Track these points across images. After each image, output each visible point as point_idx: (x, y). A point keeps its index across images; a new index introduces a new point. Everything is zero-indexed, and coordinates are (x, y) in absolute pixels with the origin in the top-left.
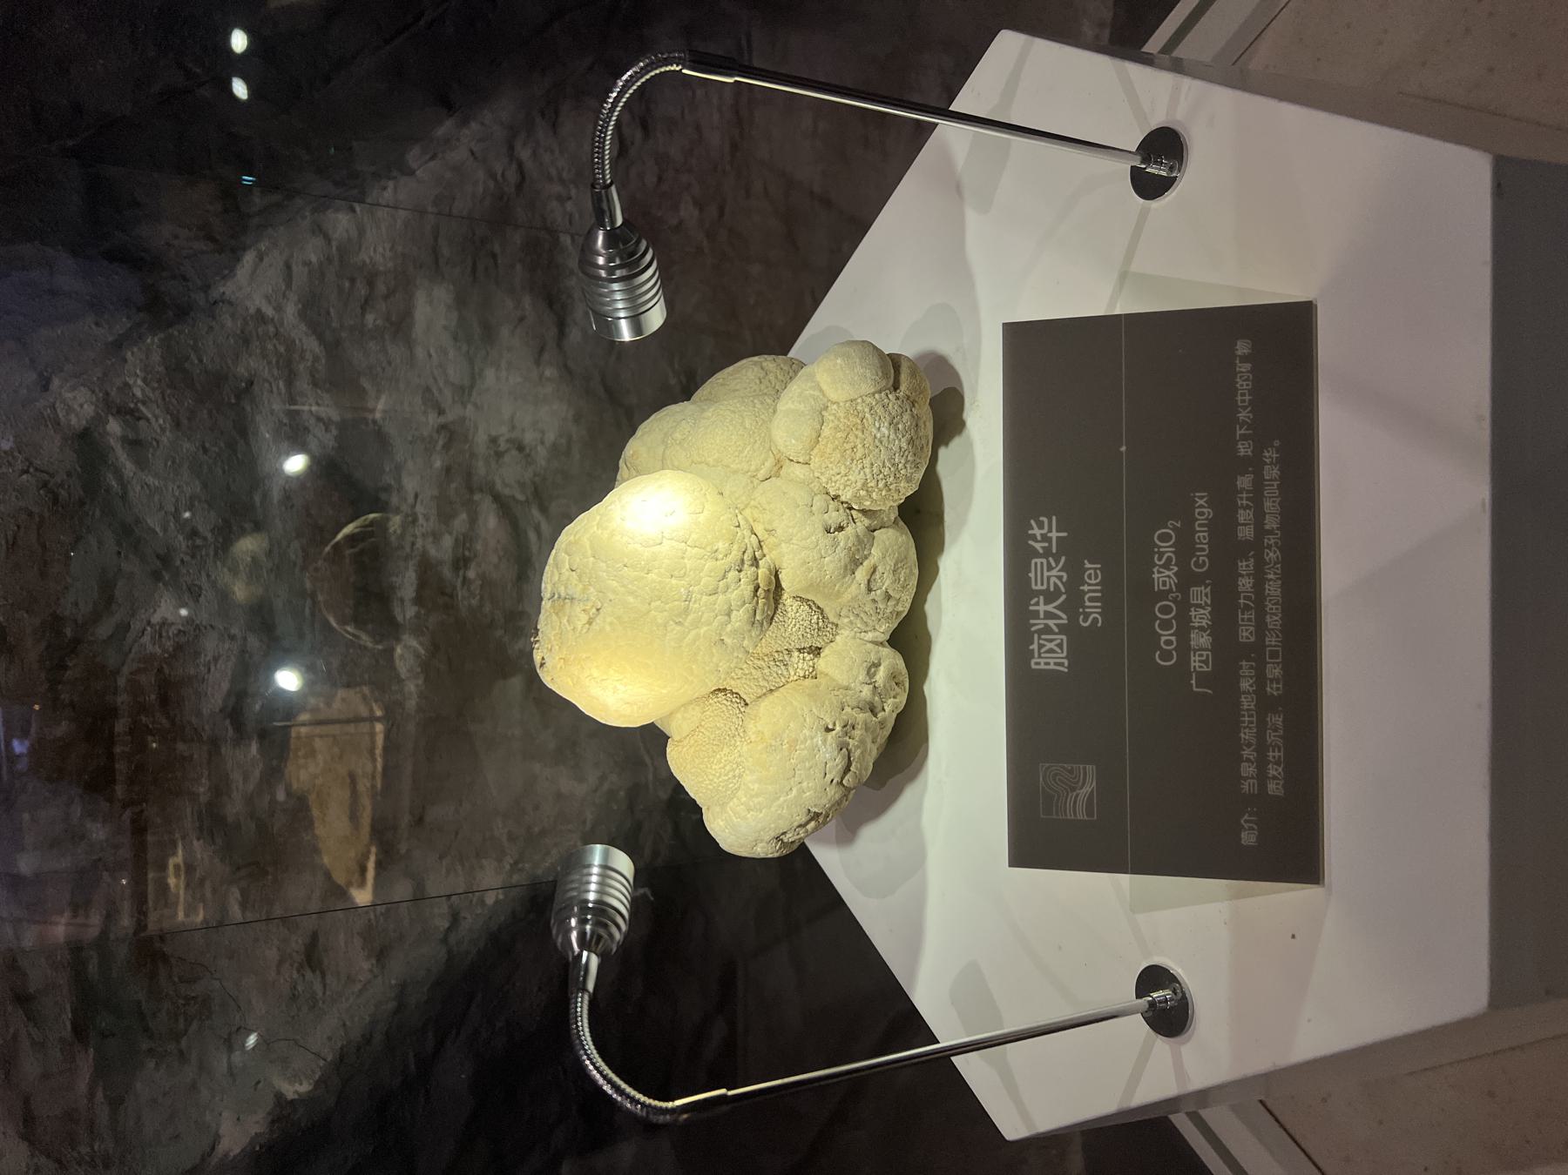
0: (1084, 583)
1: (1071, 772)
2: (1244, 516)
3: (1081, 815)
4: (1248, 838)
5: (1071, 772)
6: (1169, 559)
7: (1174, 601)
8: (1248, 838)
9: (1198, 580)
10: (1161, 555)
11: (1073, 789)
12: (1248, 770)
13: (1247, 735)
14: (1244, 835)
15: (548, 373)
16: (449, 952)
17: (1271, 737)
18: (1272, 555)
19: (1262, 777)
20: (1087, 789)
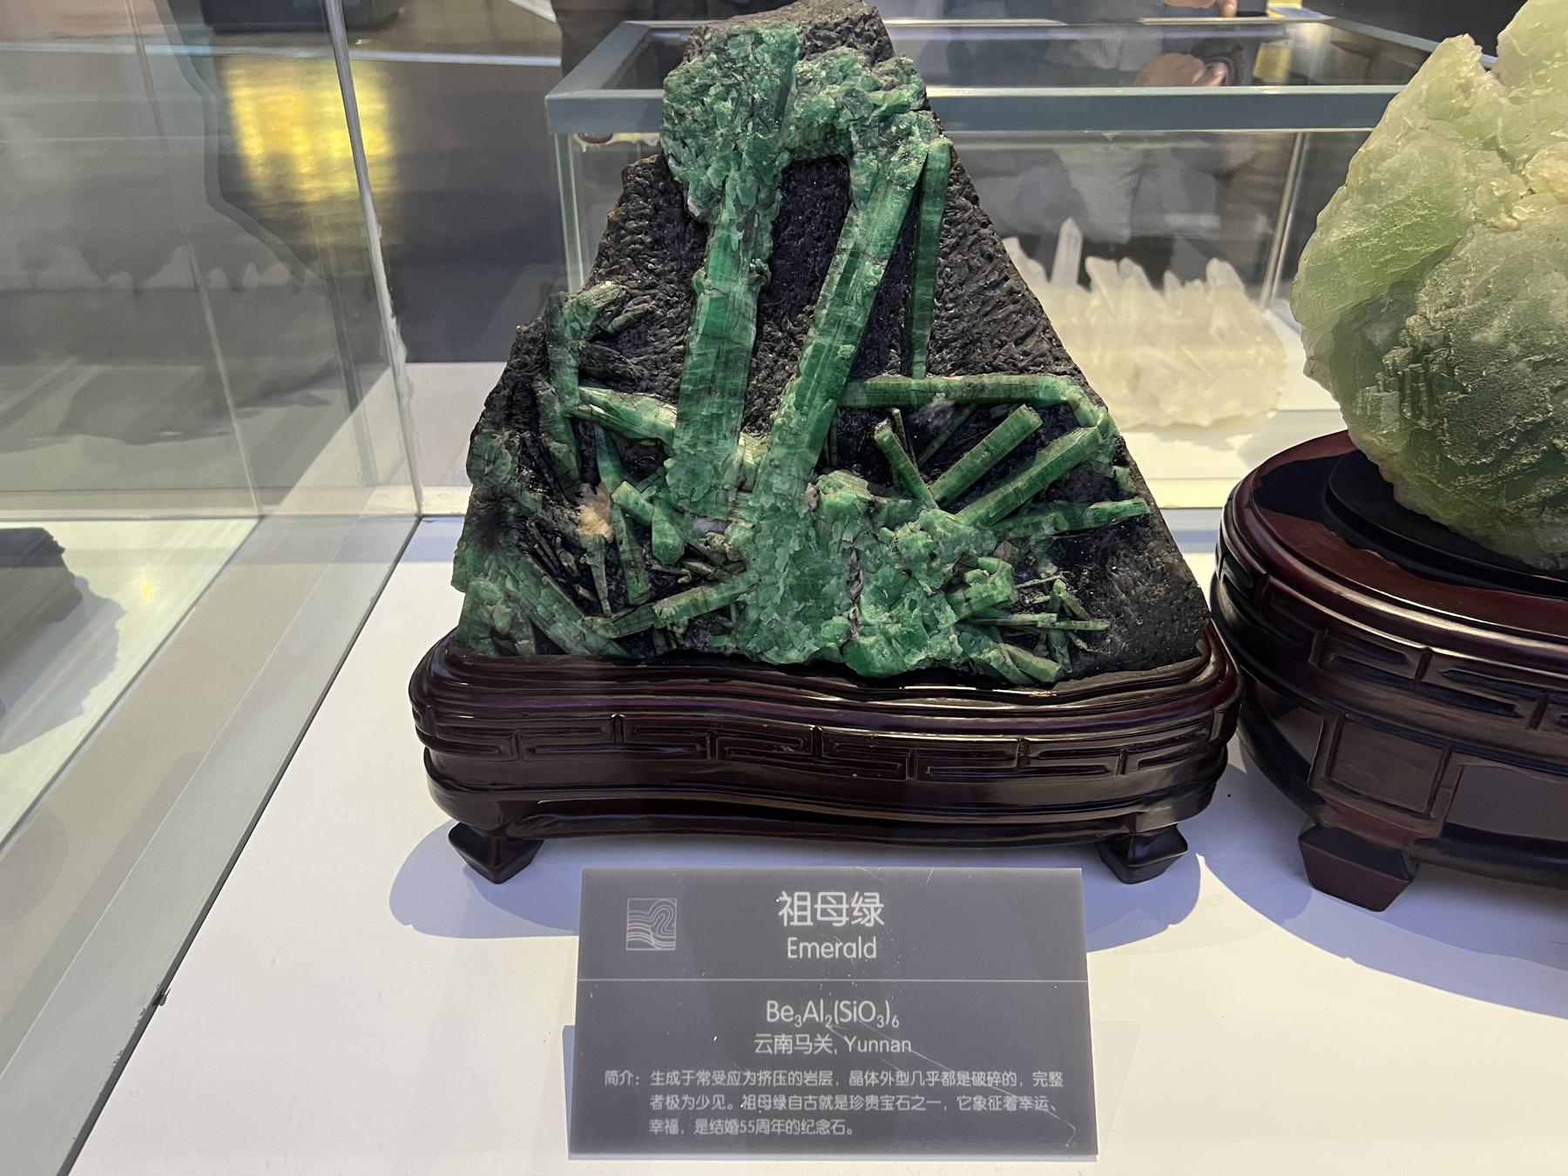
0: (791, 895)
1: (670, 927)
2: (873, 1078)
3: (630, 937)
4: (612, 1077)
5: (670, 927)
6: (845, 1016)
7: (876, 1021)
8: (612, 1077)
9: (838, 1043)
10: (850, 1008)
11: (653, 929)
12: (673, 1077)
13: (703, 1077)
14: (614, 1073)
15: (525, 472)
16: (1469, 224)
17: (872, 1100)
18: (1011, 1103)
19: (666, 1090)
20: (654, 942)
